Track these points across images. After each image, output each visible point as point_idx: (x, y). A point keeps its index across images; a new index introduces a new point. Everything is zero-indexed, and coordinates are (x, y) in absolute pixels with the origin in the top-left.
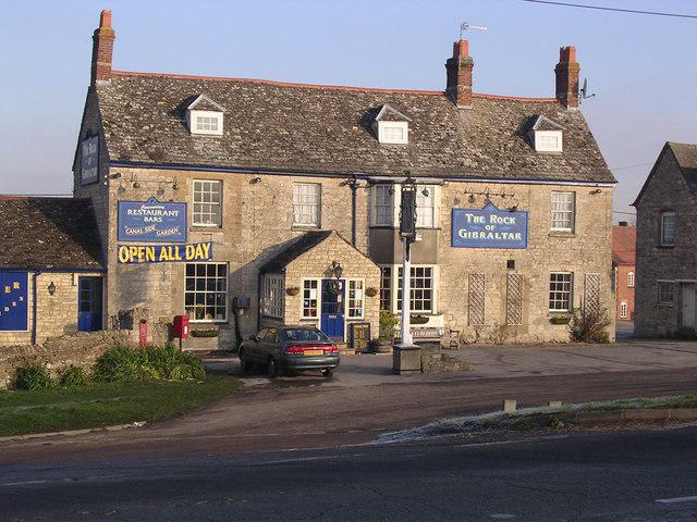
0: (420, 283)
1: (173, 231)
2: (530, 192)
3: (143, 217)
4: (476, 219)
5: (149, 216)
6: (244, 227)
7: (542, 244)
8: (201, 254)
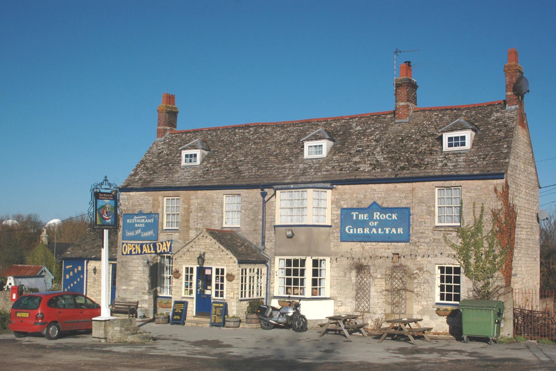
0: (449, 279)
1: (150, 233)
2: (413, 189)
3: (135, 223)
4: (361, 217)
5: (138, 223)
6: (191, 229)
7: (426, 238)
8: (165, 249)
